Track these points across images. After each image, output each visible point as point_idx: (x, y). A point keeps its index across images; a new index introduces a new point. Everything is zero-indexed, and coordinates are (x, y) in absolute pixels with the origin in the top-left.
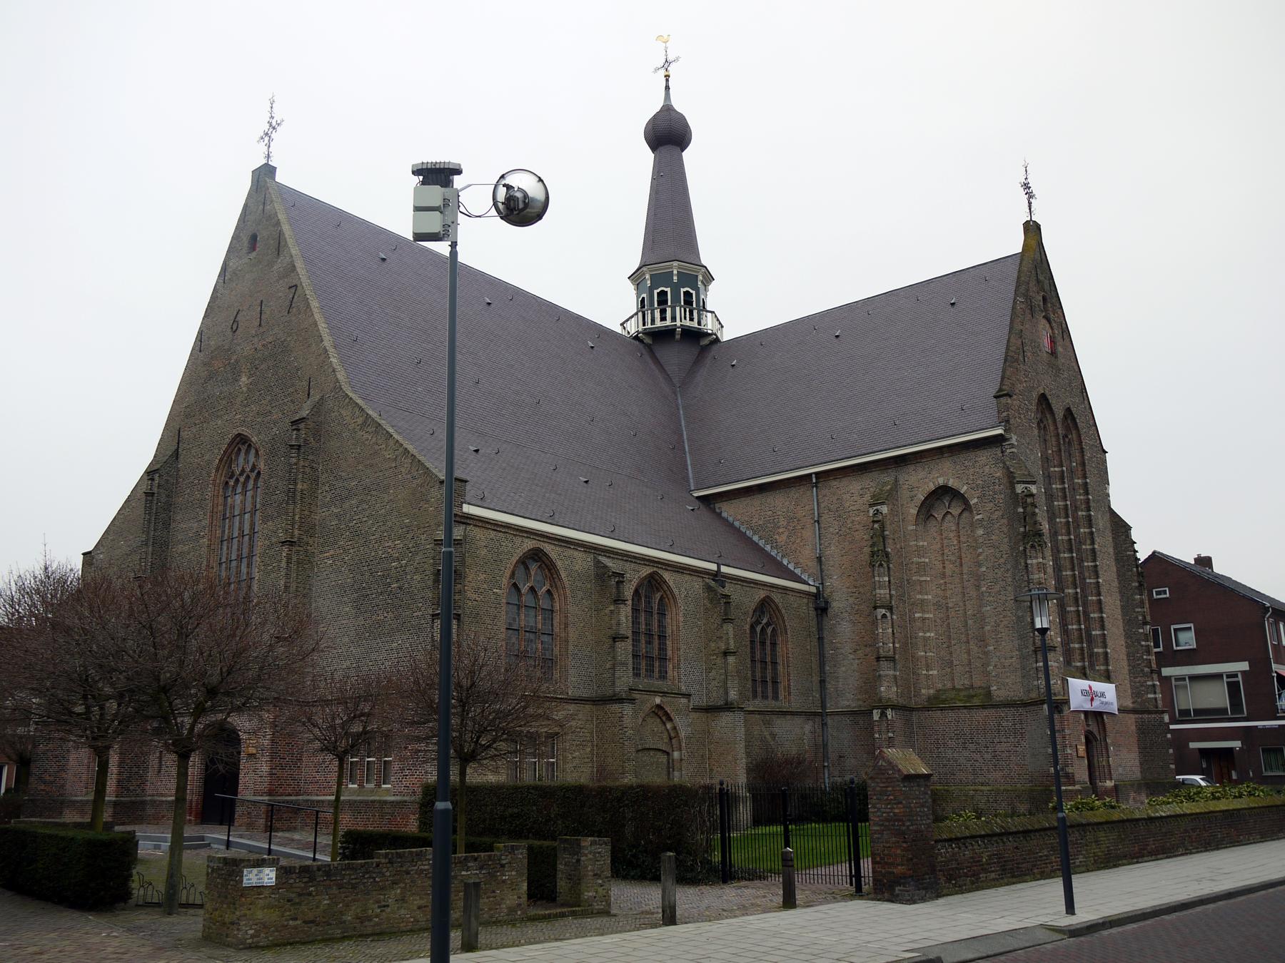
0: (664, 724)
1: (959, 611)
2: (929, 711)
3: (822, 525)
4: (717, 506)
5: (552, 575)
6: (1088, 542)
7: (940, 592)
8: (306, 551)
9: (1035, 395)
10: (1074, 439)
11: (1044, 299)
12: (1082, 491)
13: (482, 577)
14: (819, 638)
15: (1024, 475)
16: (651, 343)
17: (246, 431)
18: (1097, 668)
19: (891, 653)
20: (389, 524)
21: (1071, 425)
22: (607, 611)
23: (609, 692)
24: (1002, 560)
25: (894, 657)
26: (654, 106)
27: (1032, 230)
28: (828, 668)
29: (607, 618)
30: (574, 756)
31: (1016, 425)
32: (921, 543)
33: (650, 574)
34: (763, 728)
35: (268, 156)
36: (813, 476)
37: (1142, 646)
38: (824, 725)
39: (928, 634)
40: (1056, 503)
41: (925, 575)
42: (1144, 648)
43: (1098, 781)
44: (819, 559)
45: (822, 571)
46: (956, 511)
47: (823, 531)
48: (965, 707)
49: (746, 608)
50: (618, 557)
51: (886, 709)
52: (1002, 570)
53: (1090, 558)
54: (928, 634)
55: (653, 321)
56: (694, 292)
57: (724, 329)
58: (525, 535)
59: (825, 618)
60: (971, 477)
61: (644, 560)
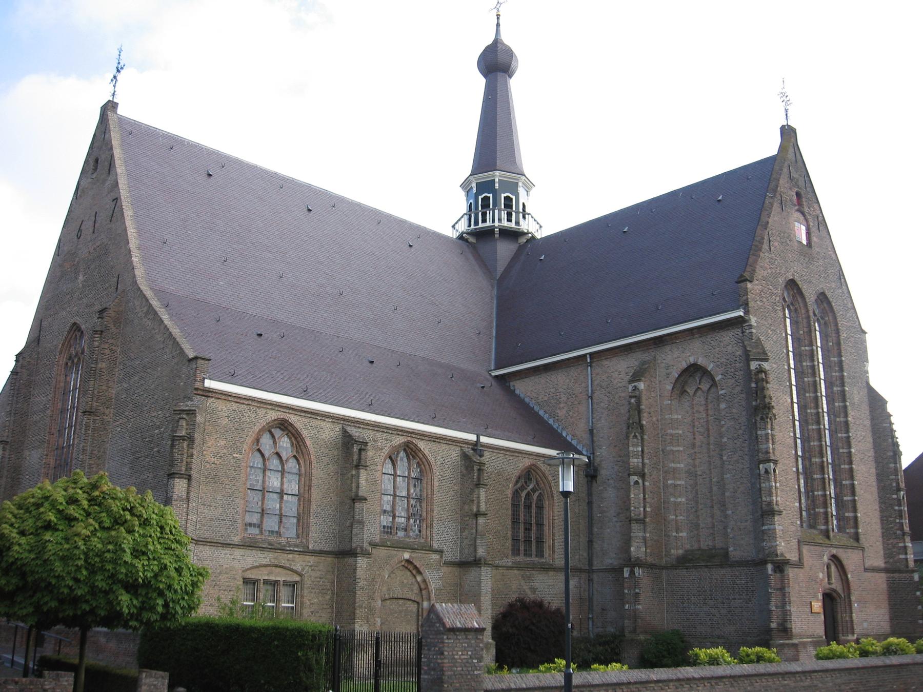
0: (415, 577)
1: (705, 478)
2: (676, 569)
3: (595, 401)
4: (512, 384)
5: (298, 442)
6: (842, 415)
7: (691, 461)
8: (103, 420)
9: (781, 281)
10: (831, 321)
11: (798, 195)
12: (837, 369)
13: (223, 443)
14: (588, 503)
15: (759, 353)
16: (475, 242)
17: (78, 320)
18: (848, 531)
19: (642, 516)
20: (156, 397)
21: (827, 308)
22: (349, 475)
23: (347, 548)
24: (741, 432)
25: (644, 521)
26: (489, 41)
27: (788, 134)
28: (596, 530)
29: (349, 482)
30: (312, 602)
31: (756, 308)
32: (676, 417)
33: (404, 443)
34: (523, 582)
35: (113, 95)
36: (588, 356)
37: (895, 510)
38: (590, 580)
39: (679, 500)
40: (806, 379)
41: (678, 445)
42: (897, 512)
43: (841, 635)
44: (591, 432)
45: (593, 441)
46: (705, 386)
47: (595, 406)
48: (706, 566)
49: (508, 475)
50: (369, 427)
51: (634, 567)
52: (740, 440)
53: (843, 429)
54: (679, 500)
55: (476, 223)
56: (513, 197)
57: (542, 229)
58: (270, 407)
59: (594, 484)
60: (717, 356)
61: (397, 430)
